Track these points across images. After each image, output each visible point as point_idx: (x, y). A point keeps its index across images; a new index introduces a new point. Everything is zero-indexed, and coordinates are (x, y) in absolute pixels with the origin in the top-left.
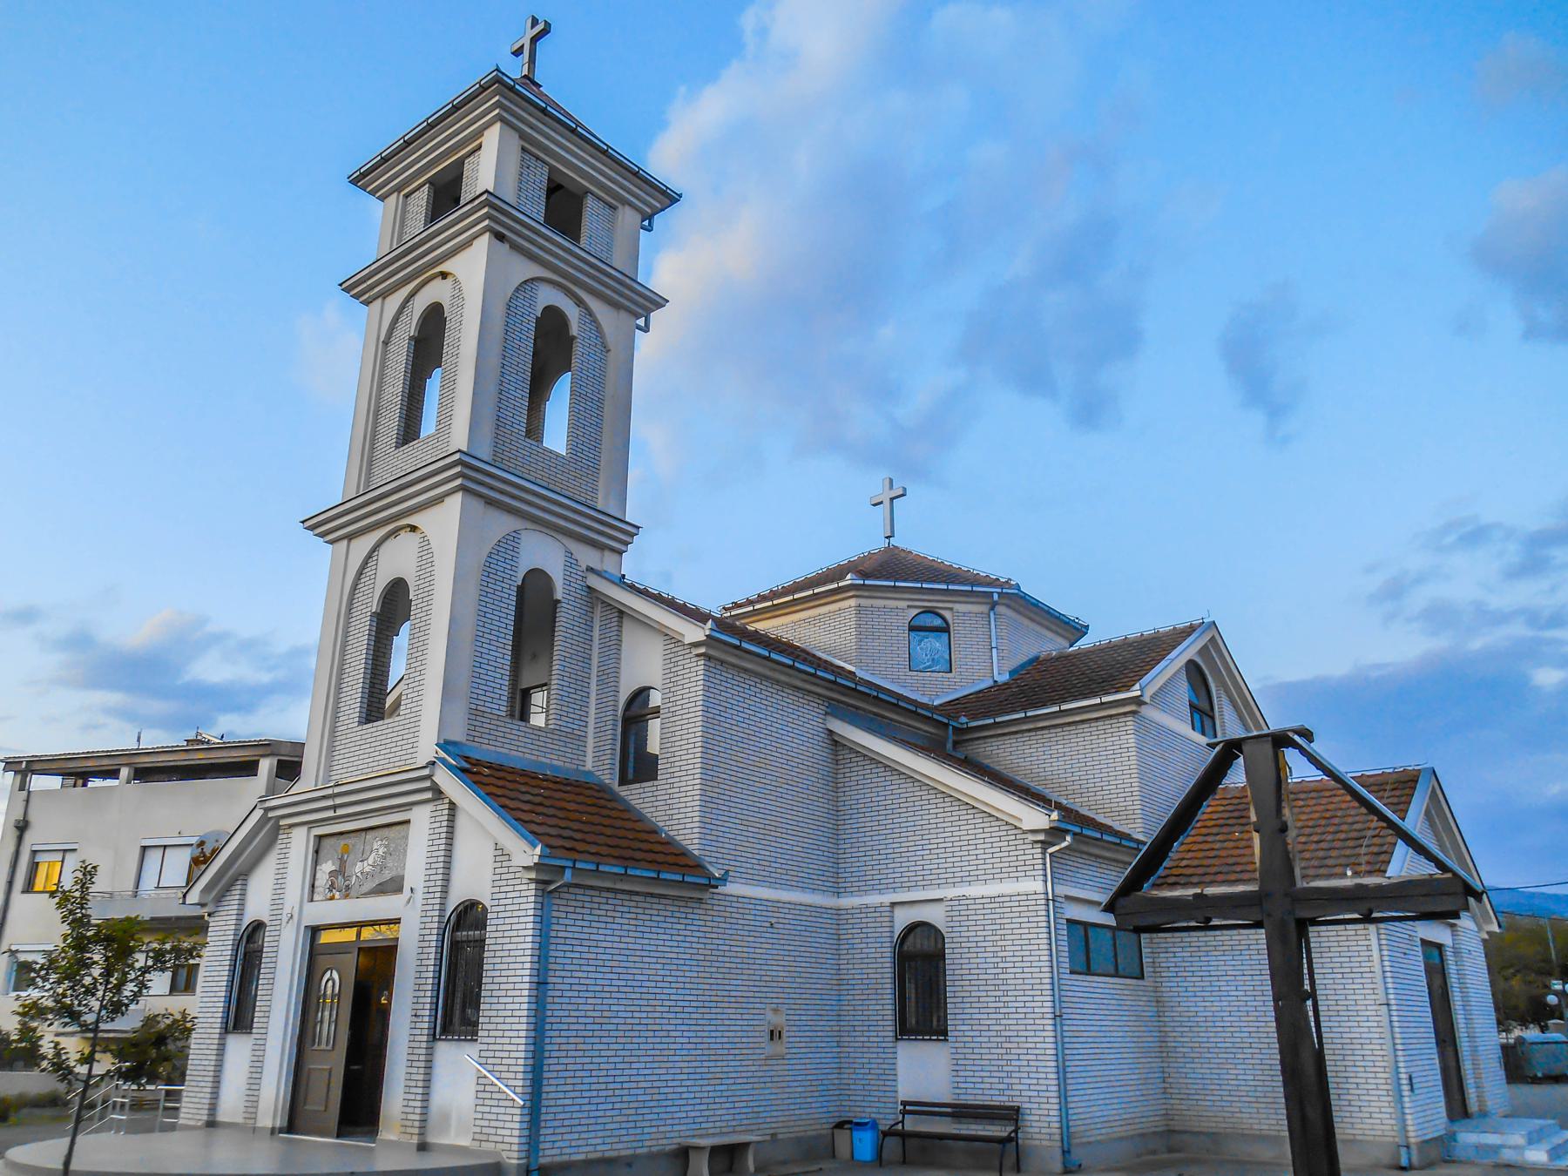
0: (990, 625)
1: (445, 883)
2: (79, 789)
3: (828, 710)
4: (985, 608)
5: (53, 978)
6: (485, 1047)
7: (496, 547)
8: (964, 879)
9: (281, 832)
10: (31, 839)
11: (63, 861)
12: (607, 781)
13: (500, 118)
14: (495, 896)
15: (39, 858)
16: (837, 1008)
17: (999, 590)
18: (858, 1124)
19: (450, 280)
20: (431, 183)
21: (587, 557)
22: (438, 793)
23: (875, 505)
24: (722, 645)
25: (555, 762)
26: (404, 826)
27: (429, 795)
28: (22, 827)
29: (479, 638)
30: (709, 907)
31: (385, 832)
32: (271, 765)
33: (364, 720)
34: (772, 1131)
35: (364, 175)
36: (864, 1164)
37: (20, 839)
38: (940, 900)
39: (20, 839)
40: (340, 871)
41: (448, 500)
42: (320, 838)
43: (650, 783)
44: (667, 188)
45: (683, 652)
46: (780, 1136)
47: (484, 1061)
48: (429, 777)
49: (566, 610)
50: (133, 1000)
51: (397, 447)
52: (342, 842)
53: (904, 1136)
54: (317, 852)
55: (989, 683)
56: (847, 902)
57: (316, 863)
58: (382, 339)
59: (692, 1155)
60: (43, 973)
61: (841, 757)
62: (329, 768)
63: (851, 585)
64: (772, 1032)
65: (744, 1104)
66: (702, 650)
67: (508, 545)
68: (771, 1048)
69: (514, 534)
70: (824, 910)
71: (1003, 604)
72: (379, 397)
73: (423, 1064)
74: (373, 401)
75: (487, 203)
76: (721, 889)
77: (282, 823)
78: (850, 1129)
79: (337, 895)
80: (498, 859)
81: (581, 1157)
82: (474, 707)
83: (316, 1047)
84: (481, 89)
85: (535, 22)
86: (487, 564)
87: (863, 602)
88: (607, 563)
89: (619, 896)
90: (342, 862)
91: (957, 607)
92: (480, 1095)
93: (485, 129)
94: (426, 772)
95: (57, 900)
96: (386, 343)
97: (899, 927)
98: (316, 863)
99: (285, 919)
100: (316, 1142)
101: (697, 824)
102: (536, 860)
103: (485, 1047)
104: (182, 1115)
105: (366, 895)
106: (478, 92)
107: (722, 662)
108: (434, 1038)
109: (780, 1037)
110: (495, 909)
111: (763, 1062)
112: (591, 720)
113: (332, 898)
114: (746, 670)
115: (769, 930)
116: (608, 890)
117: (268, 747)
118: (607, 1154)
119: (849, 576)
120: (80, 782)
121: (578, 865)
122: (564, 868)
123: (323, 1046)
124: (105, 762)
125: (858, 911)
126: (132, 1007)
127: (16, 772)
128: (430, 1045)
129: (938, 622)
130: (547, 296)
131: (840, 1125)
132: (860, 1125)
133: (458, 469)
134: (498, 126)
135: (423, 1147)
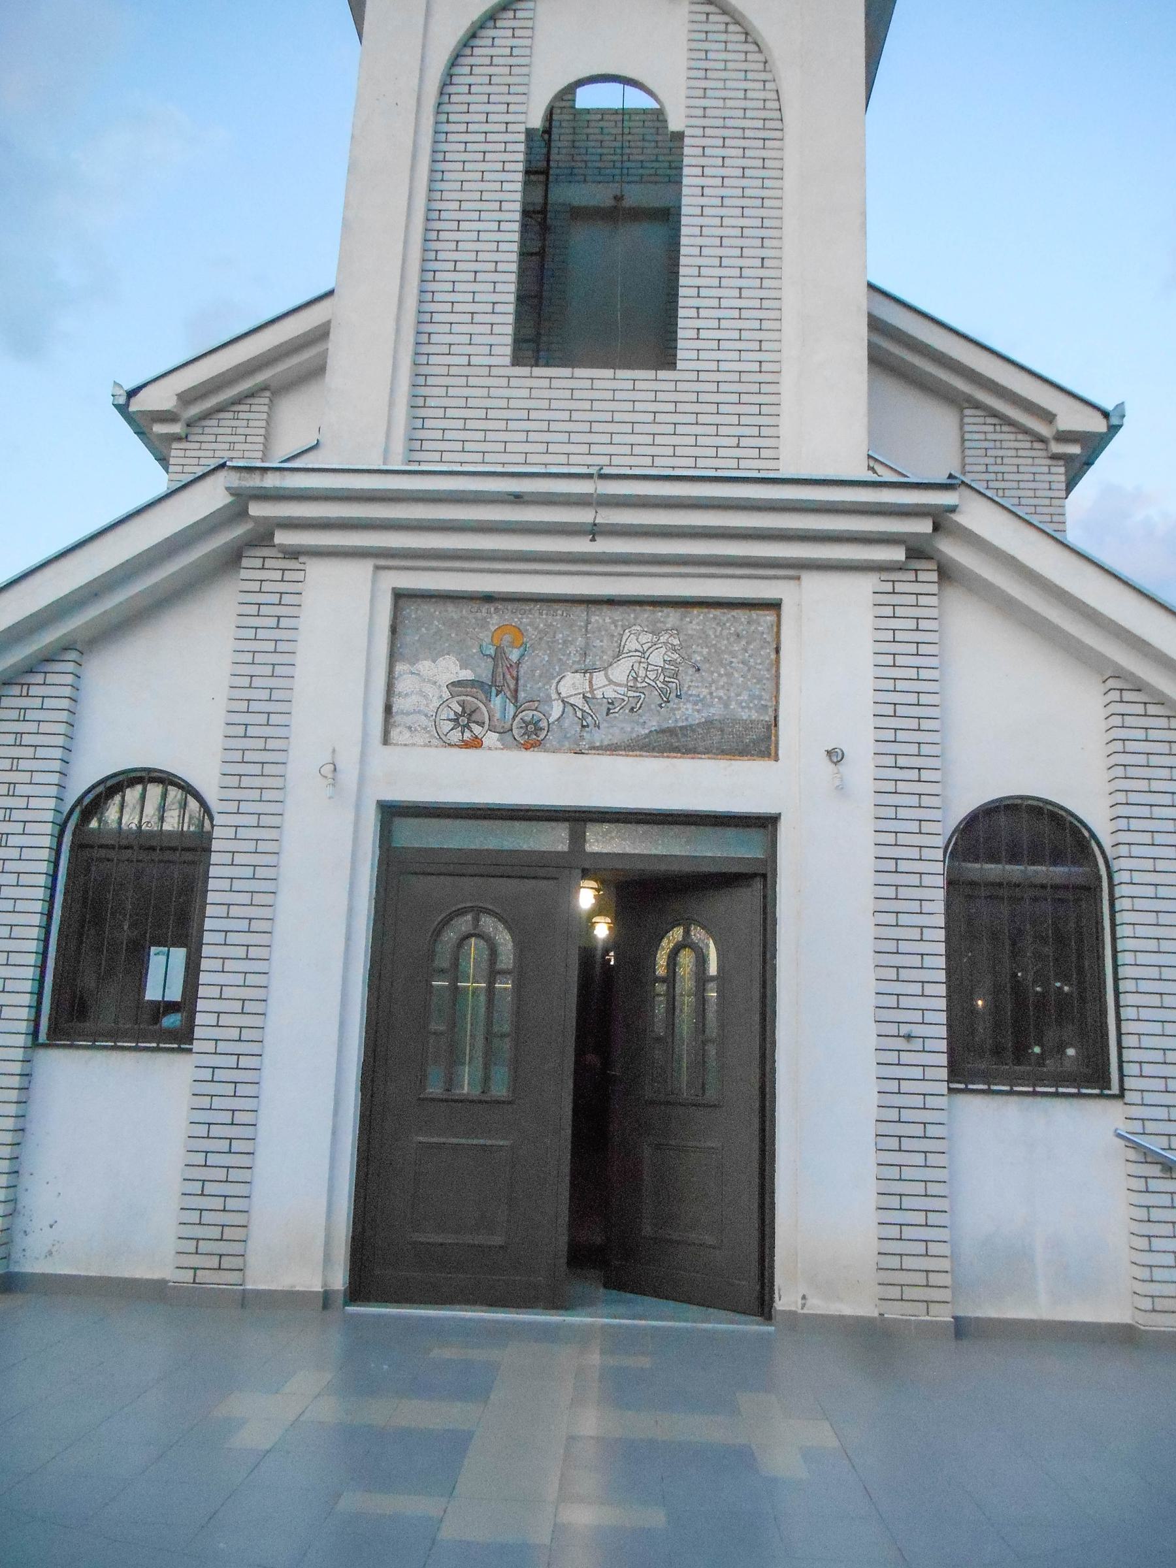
27: (898, 554)
31: (672, 617)
42: (400, 596)
105: (612, 749)
113: (475, 743)
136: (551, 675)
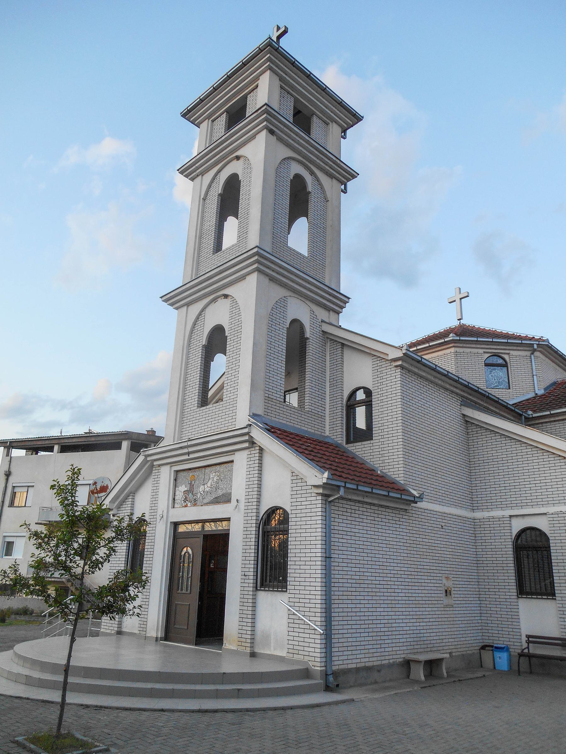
0: (531, 362)
1: (259, 497)
2: (34, 456)
3: (462, 403)
4: (528, 353)
5: (53, 543)
6: (293, 596)
7: (275, 305)
8: (508, 505)
9: (154, 469)
10: (11, 479)
11: (27, 492)
12: (340, 442)
13: (270, 68)
14: (293, 504)
15: (16, 490)
16: (477, 577)
17: (538, 343)
18: (496, 648)
19: (242, 160)
20: (227, 112)
21: (322, 314)
22: (252, 443)
23: (450, 303)
24: (410, 360)
25: (309, 430)
26: (230, 465)
27: (246, 445)
28: (8, 475)
29: (268, 356)
30: (411, 515)
31: (218, 468)
32: (128, 444)
33: (200, 405)
34: (449, 651)
35: (189, 111)
36: (502, 673)
37: (7, 480)
38: (545, 514)
39: (7, 480)
40: (191, 491)
41: (248, 278)
42: (177, 472)
43: (369, 442)
44: (356, 112)
45: (386, 365)
46: (454, 654)
47: (292, 604)
48: (248, 434)
49: (312, 344)
50: (106, 560)
51: (213, 254)
52: (191, 474)
53: (530, 656)
54: (175, 480)
55: (531, 395)
56: (478, 515)
57: (175, 486)
58: (202, 197)
59: (412, 666)
60: (46, 540)
61: (470, 431)
62: (181, 432)
63: (453, 340)
64: (446, 590)
65: (435, 634)
66: (400, 363)
67: (281, 305)
68: (446, 601)
69: (285, 299)
70: (467, 519)
71: (539, 351)
72: (201, 229)
73: (251, 605)
74: (198, 231)
75: (266, 112)
76: (419, 505)
77: (155, 463)
78: (492, 650)
79: (189, 504)
80: (294, 481)
81: (354, 666)
82: (267, 395)
83: (179, 591)
84: (260, 51)
85: (278, 28)
86: (271, 314)
87: (458, 350)
88: (332, 317)
89: (365, 506)
90: (191, 485)
91: (511, 352)
92: (291, 625)
93: (261, 75)
94: (246, 430)
95: (55, 491)
96: (204, 199)
97: (515, 532)
98: (175, 486)
99: (159, 518)
100: (175, 645)
101: (402, 465)
102: (325, 481)
103: (293, 596)
104: (102, 627)
105: (207, 504)
106: (258, 53)
107: (409, 371)
108: (256, 589)
109: (450, 595)
110: (293, 512)
111: (443, 609)
112: (327, 407)
113: (186, 506)
114: (421, 377)
115: (441, 530)
116: (359, 502)
117: (126, 435)
118: (367, 664)
119: (451, 335)
120: (34, 453)
121: (348, 485)
122: (339, 487)
123: (184, 591)
124: (47, 442)
125: (488, 520)
126: (106, 564)
127: (5, 447)
128: (255, 593)
129: (500, 361)
130: (296, 169)
131: (483, 648)
132: (498, 649)
133: (256, 258)
134: (268, 72)
135: (253, 655)
136: (199, 487)
